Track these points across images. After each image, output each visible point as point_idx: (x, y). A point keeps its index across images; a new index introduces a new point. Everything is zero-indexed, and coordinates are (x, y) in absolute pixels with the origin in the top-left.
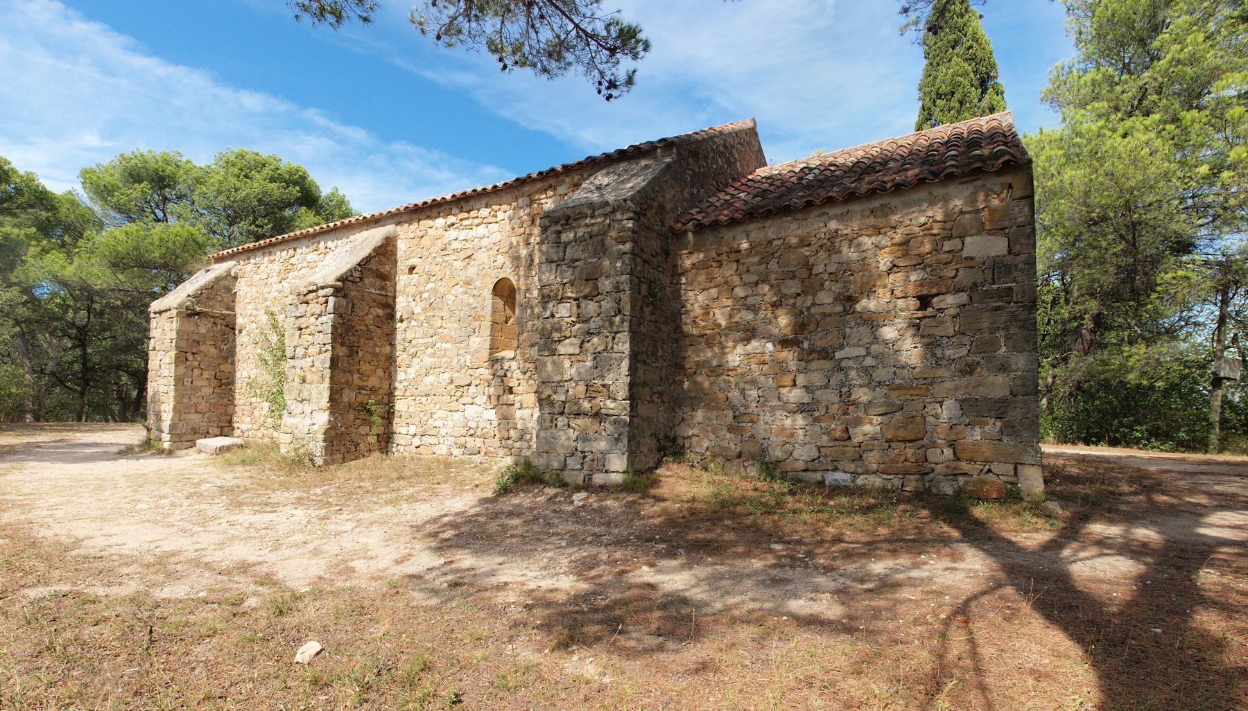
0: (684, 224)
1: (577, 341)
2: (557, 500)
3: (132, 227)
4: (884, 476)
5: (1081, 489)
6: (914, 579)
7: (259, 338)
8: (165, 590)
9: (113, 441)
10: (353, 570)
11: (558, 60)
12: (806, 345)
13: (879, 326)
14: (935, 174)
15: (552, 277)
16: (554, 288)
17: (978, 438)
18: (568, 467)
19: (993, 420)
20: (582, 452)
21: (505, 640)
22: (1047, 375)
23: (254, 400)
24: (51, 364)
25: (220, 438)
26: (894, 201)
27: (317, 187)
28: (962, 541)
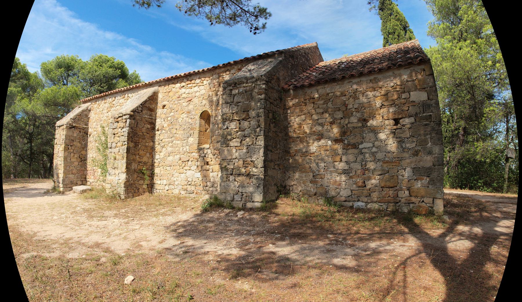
2: (230, 215)
3: (54, 87)
4: (380, 204)
5: (458, 210)
6: (387, 250)
8: (70, 254)
9: (42, 187)
10: (141, 246)
12: (346, 142)
13: (378, 133)
14: (394, 65)
15: (228, 110)
16: (228, 115)
17: (420, 186)
18: (235, 200)
19: (426, 178)
20: (241, 193)
22: (447, 156)
23: (95, 168)
24: (19, 151)
25: (82, 186)
26: (379, 76)
27: (128, 70)
28: (409, 233)
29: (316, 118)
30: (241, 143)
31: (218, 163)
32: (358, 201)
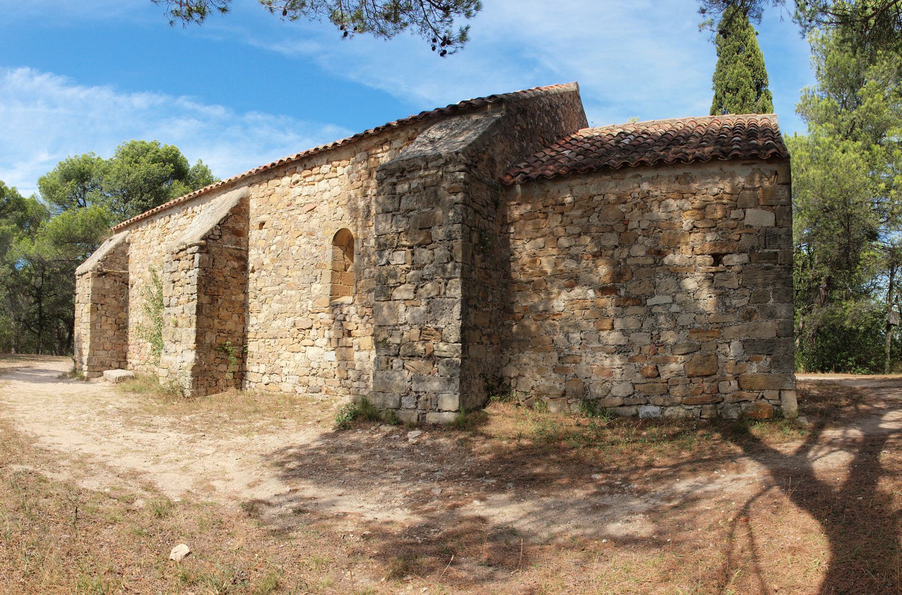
0: (513, 177)
1: (411, 287)
2: (393, 437)
4: (687, 407)
5: (820, 406)
7: (145, 291)
9: (56, 369)
11: (395, 22)
12: (622, 292)
13: (683, 278)
14: (725, 154)
15: (388, 227)
16: (389, 236)
19: (765, 357)
20: (416, 392)
21: (344, 566)
22: (800, 321)
23: (141, 340)
26: (694, 172)
27: (186, 162)
28: (744, 456)
29: (566, 245)
30: (415, 293)
31: (371, 333)
32: (646, 404)
